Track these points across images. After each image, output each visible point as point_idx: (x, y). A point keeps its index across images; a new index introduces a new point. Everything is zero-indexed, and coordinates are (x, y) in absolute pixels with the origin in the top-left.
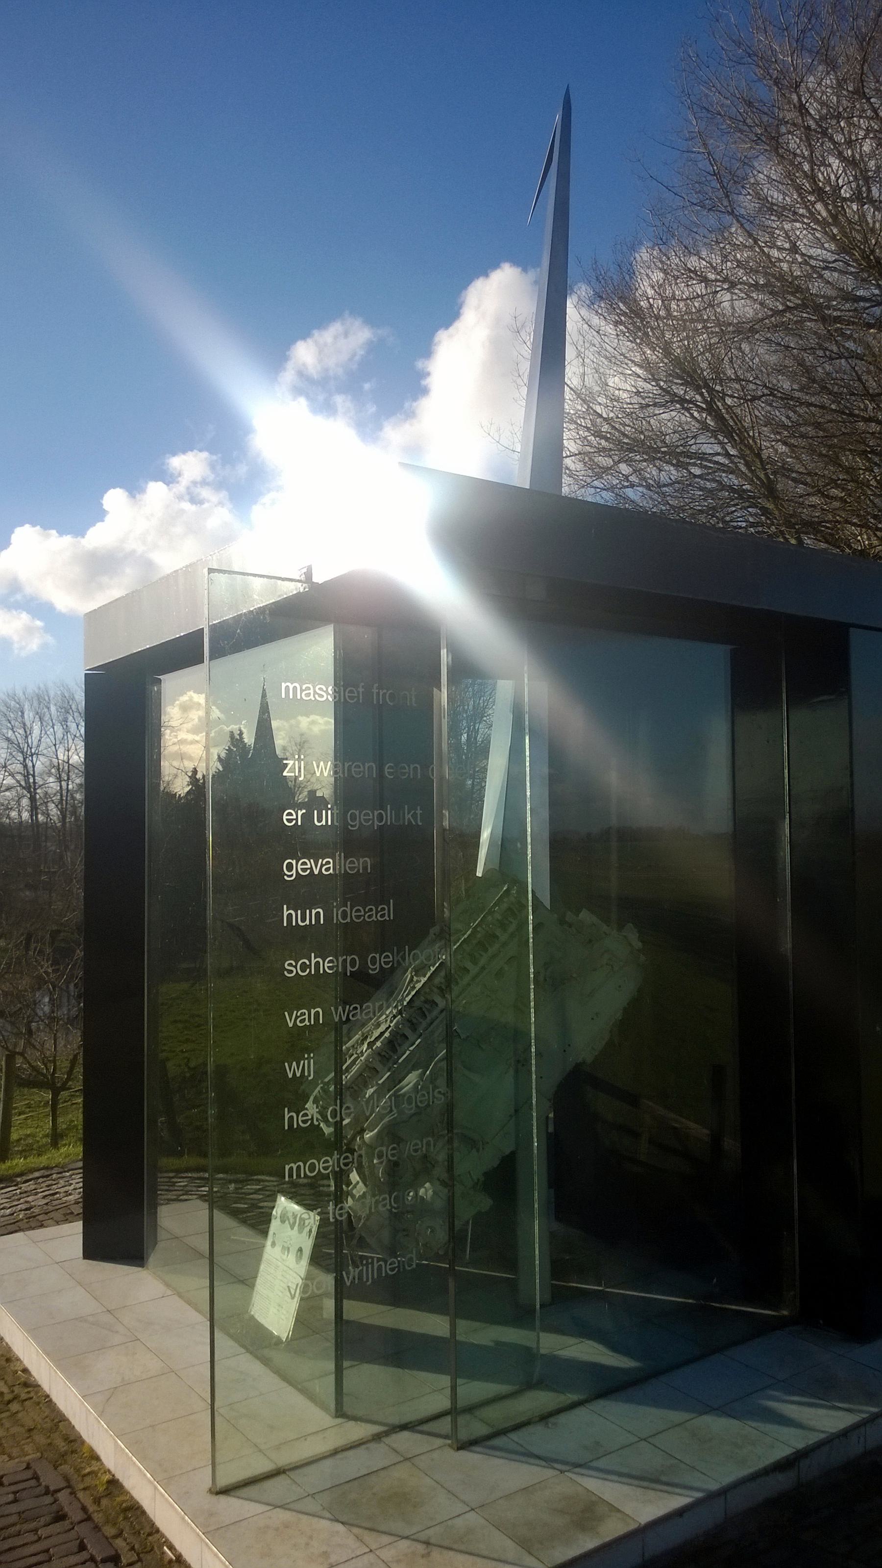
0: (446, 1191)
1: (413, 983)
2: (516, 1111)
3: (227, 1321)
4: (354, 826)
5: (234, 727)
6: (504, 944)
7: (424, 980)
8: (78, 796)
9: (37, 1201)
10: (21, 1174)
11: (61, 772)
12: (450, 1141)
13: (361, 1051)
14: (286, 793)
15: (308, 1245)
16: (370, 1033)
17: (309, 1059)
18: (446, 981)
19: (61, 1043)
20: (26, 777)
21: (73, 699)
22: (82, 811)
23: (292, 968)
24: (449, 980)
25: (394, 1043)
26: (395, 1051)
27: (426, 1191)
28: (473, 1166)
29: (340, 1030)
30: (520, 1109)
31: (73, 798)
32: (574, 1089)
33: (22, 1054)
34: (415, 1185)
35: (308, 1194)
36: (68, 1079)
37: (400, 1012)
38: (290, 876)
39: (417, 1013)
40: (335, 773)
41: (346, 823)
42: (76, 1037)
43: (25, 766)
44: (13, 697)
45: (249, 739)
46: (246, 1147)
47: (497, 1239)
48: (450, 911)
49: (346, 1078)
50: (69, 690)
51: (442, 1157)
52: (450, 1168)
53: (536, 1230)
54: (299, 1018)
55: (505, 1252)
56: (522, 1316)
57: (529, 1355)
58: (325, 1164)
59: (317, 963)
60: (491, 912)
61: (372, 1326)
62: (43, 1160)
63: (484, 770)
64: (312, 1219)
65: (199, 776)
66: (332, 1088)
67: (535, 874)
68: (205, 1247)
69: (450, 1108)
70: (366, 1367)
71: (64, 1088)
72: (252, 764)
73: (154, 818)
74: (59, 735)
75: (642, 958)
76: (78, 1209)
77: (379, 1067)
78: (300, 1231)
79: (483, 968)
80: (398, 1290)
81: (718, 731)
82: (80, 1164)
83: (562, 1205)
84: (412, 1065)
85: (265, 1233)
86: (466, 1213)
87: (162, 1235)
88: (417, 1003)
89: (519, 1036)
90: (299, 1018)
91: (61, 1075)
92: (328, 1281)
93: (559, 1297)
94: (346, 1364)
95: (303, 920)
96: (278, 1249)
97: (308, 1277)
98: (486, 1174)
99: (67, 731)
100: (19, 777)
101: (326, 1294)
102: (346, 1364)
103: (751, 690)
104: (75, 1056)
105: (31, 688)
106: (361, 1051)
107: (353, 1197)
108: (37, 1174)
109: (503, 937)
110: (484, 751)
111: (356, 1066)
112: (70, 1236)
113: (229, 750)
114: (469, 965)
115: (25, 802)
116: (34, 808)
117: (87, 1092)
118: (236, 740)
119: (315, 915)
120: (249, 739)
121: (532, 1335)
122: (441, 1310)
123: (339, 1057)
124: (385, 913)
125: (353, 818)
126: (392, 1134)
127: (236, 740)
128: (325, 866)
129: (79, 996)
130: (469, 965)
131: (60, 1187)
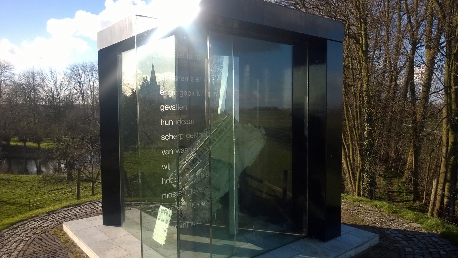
0: (209, 203)
1: (199, 144)
2: (229, 180)
3: (145, 239)
4: (182, 96)
5: (145, 76)
6: (226, 133)
7: (202, 143)
8: (97, 96)
9: (89, 210)
10: (84, 203)
11: (91, 89)
12: (210, 188)
13: (184, 164)
14: (161, 101)
15: (169, 219)
16: (187, 159)
17: (169, 164)
18: (210, 142)
19: (94, 168)
20: (81, 90)
21: (94, 66)
22: (98, 101)
23: (164, 138)
24: (210, 143)
25: (194, 161)
26: (194, 163)
27: (203, 203)
28: (217, 196)
29: (179, 156)
30: (230, 179)
31: (95, 97)
32: (245, 175)
33: (82, 172)
34: (201, 200)
35: (168, 204)
36: (97, 179)
37: (196, 152)
38: (163, 110)
39: (199, 154)
40: (176, 79)
41: (179, 95)
42: (99, 167)
43: (80, 87)
44: (75, 66)
45: (149, 79)
46: (150, 194)
47: (223, 216)
48: (211, 121)
49: (180, 171)
50: (93, 64)
51: (208, 193)
52: (210, 197)
53: (235, 214)
54: (166, 152)
55: (226, 220)
56: (231, 237)
57: (232, 248)
58: (174, 195)
59: (171, 137)
60: (222, 124)
61: (189, 241)
62: (90, 199)
63: (220, 89)
64: (170, 212)
65: (134, 91)
66: (176, 174)
67: (235, 114)
68: (139, 221)
69: (210, 179)
70: (186, 252)
71: (95, 182)
72: (150, 86)
73: (120, 102)
74: (91, 77)
75: (265, 137)
76: (101, 212)
77: (189, 168)
78: (167, 215)
79: (220, 140)
80: (196, 230)
81: (288, 75)
82: (101, 200)
83: (242, 209)
84: (199, 167)
85: (156, 218)
86: (215, 209)
87: (126, 218)
88: (200, 150)
89: (231, 165)
90: (166, 152)
91: (95, 178)
92: (175, 230)
93: (241, 232)
94: (181, 251)
95: (167, 123)
96: (160, 221)
97: (169, 229)
98: (220, 198)
99: (93, 76)
100: (78, 90)
101: (175, 233)
102: (181, 251)
103: (298, 61)
104: (99, 172)
105: (81, 63)
106: (184, 164)
107: (182, 206)
108: (88, 203)
109: (226, 131)
110: (219, 84)
111: (183, 169)
112: (100, 219)
113: (143, 83)
114: (216, 139)
115: (81, 98)
116: (83, 100)
117: (103, 183)
118: (145, 80)
119: (170, 122)
120: (149, 79)
121: (234, 242)
122: (208, 236)
123: (178, 166)
124: (192, 122)
125: (181, 93)
126: (193, 186)
127: (145, 80)
128: (173, 108)
129: (99, 155)
130: (216, 139)
131: (96, 206)
